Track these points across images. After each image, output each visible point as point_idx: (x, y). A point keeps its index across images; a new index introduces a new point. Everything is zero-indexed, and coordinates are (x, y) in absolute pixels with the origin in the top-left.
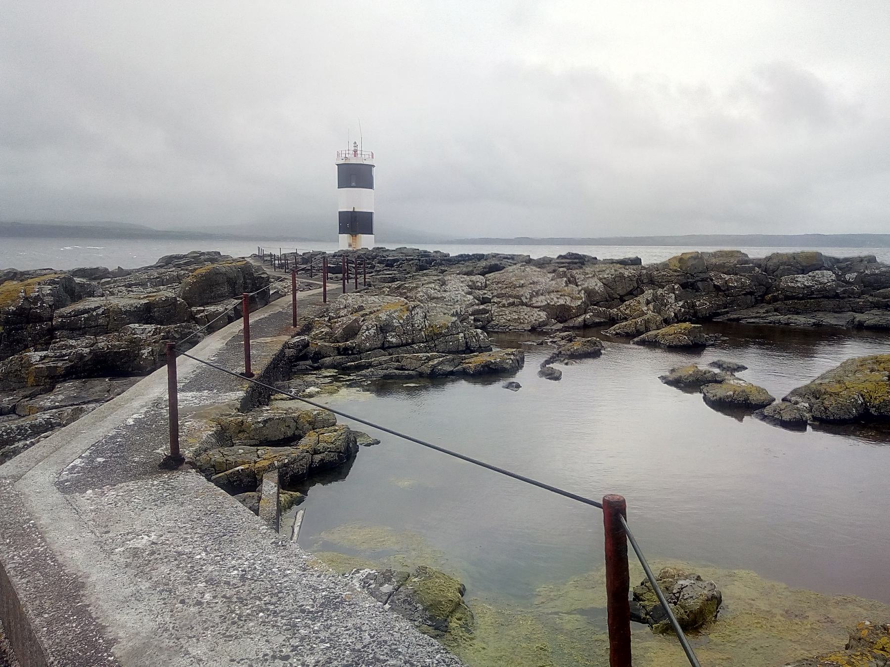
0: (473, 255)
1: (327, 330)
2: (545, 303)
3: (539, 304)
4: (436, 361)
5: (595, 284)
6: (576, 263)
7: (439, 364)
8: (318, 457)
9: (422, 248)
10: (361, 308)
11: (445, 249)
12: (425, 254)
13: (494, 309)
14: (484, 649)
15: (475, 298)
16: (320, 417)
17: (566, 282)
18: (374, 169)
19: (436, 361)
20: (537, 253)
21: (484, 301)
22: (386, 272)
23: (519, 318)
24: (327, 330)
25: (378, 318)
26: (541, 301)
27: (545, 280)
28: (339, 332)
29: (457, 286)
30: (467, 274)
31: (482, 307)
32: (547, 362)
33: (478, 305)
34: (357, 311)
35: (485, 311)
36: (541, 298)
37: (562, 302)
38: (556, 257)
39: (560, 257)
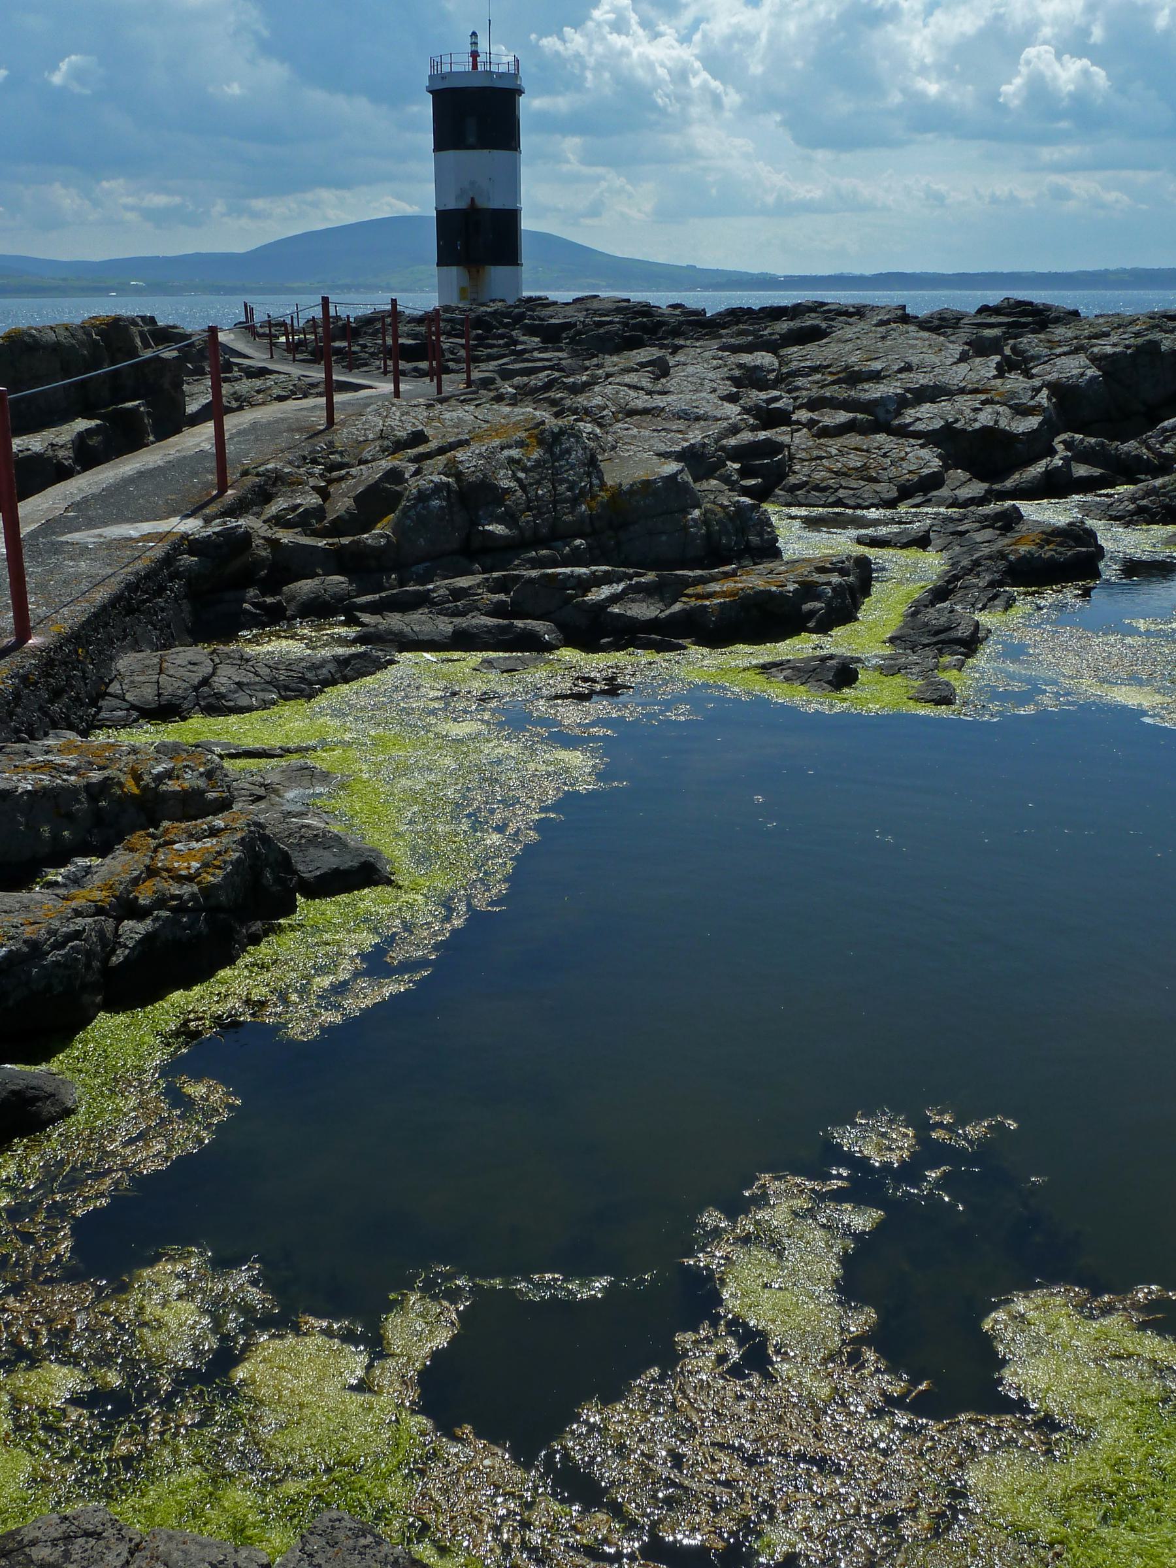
0: (762, 309)
1: (314, 500)
2: (938, 424)
3: (920, 426)
4: (605, 591)
5: (1074, 368)
6: (1025, 325)
7: (614, 599)
8: (134, 930)
9: (637, 296)
10: (418, 438)
11: (693, 299)
12: (646, 310)
13: (801, 440)
14: (791, 1427)
15: (746, 410)
16: (172, 786)
17: (999, 367)
18: (522, 100)
19: (605, 591)
20: (922, 303)
21: (770, 418)
22: (536, 354)
23: (865, 467)
24: (314, 500)
25: (452, 469)
26: (927, 416)
27: (941, 360)
28: (342, 505)
29: (699, 381)
30: (735, 349)
31: (762, 435)
32: (940, 594)
33: (753, 429)
34: (399, 446)
35: (773, 447)
36: (926, 409)
37: (985, 418)
38: (973, 310)
39: (984, 310)
